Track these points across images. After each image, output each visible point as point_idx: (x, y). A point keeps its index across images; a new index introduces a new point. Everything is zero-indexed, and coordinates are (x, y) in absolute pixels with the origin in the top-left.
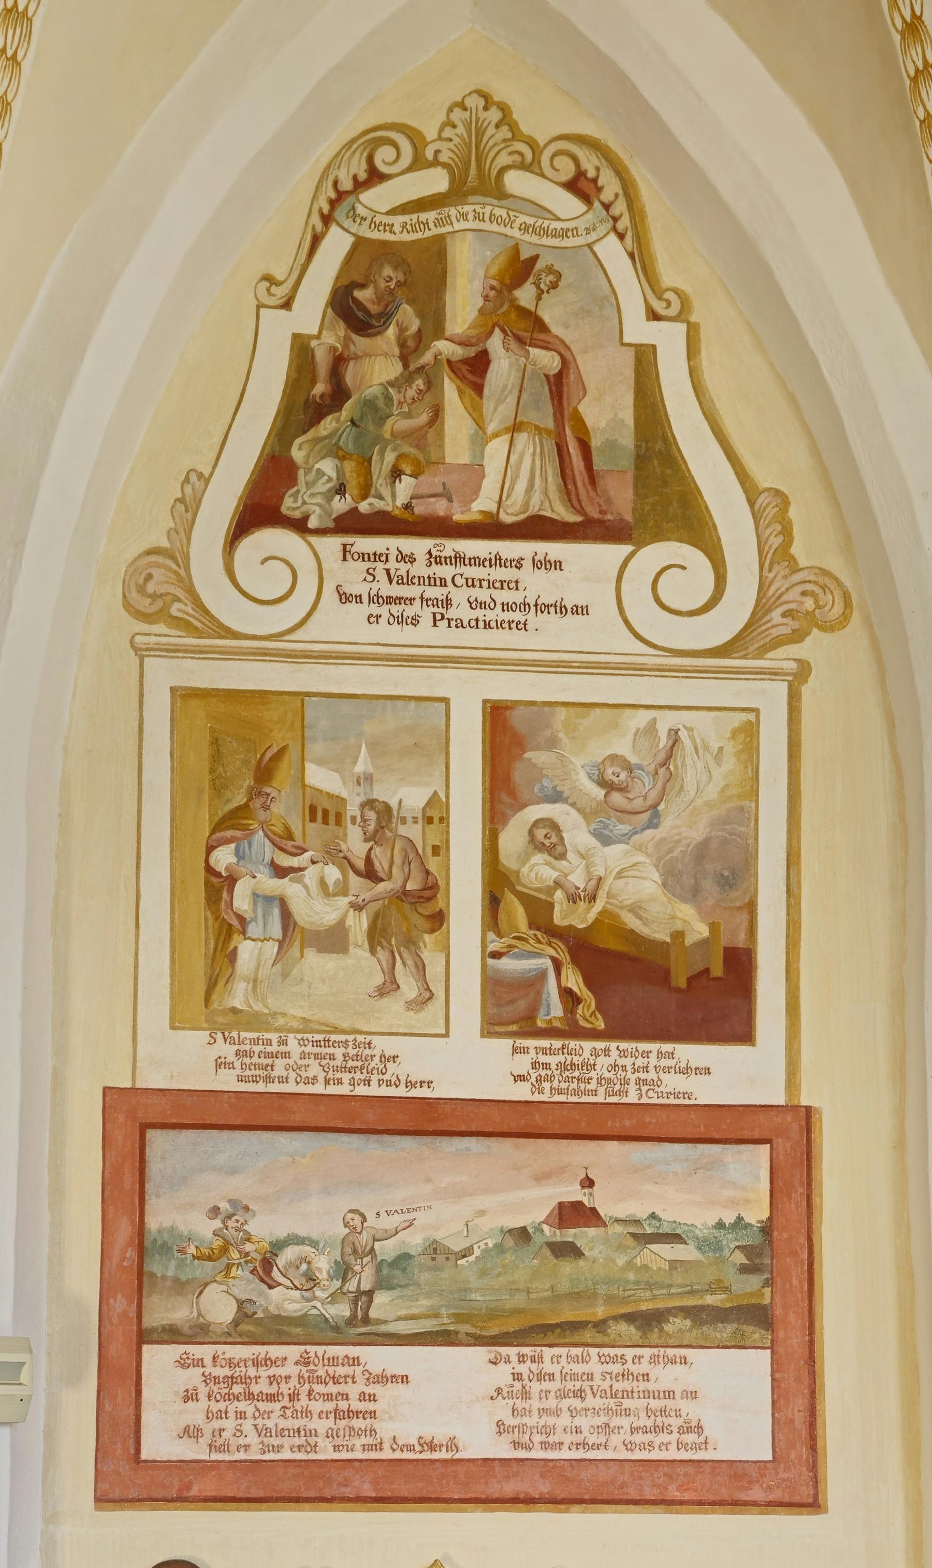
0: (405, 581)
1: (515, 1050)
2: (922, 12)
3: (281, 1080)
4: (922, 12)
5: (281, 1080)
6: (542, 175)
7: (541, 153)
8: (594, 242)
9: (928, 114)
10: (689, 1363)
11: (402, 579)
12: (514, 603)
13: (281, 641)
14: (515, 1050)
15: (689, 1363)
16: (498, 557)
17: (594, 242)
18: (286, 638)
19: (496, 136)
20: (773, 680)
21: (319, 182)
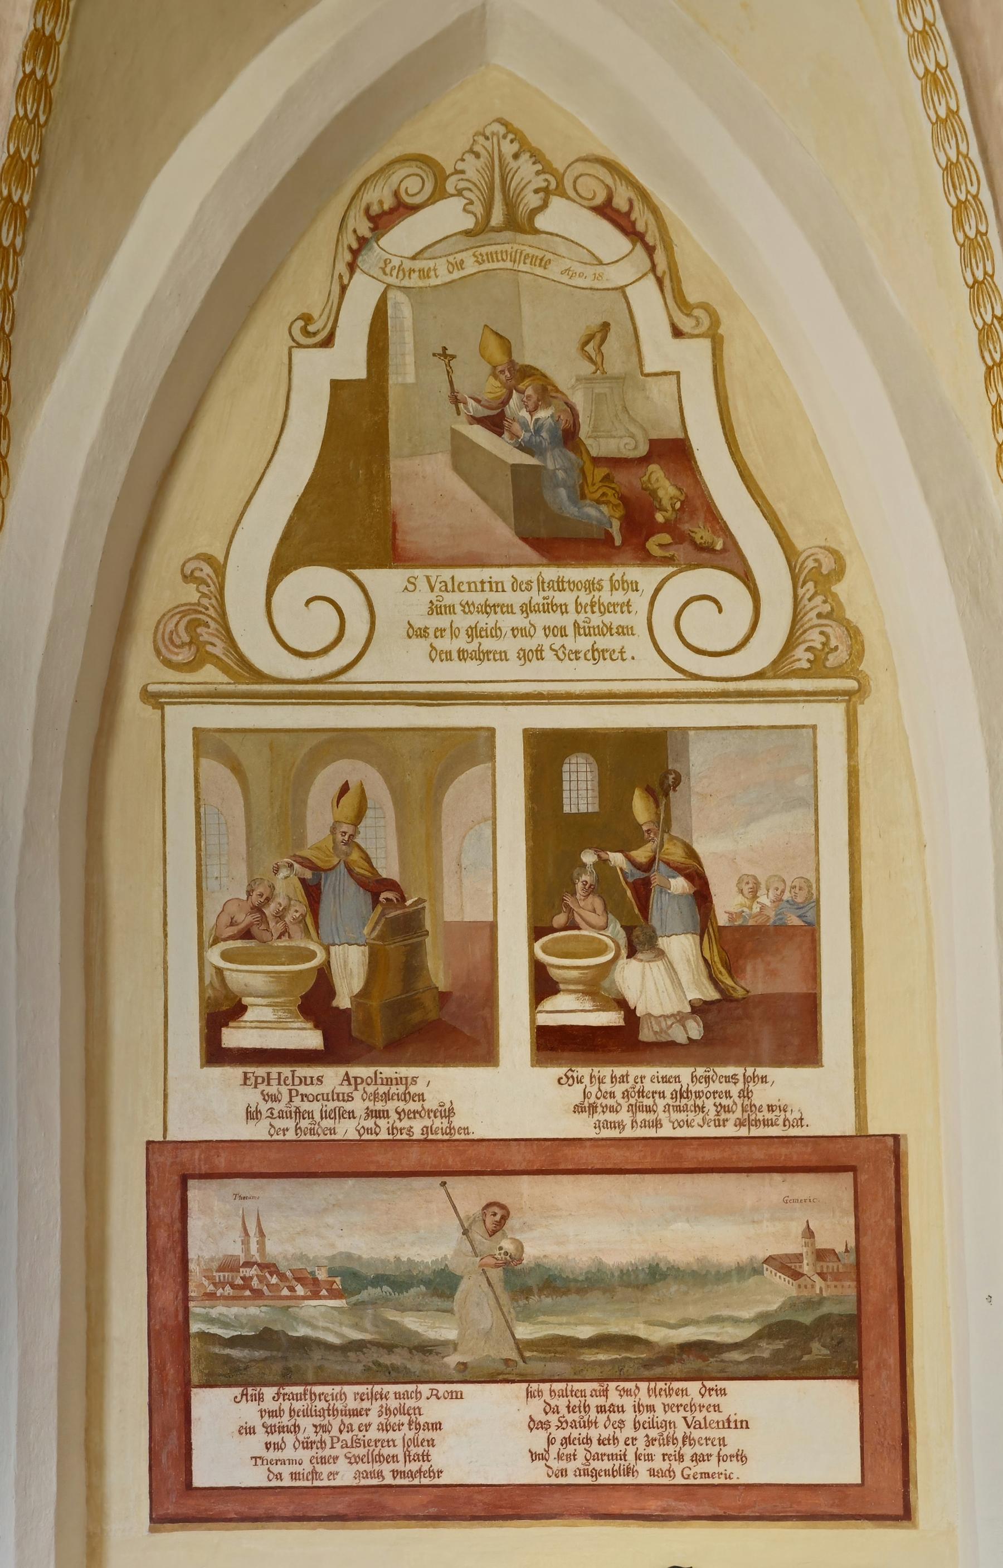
0: (703, 1425)
1: (529, 1394)
2: (958, 107)
3: (305, 1445)
4: (958, 107)
5: (305, 1445)
6: (568, 198)
7: (563, 179)
8: (626, 286)
9: (1001, 400)
10: (641, 591)
11: (700, 1424)
12: (555, 626)
13: (337, 683)
14: (529, 1394)
15: (641, 591)
16: (541, 579)
17: (626, 286)
18: (342, 678)
19: (525, 170)
20: (938, 33)
21: (372, 176)
